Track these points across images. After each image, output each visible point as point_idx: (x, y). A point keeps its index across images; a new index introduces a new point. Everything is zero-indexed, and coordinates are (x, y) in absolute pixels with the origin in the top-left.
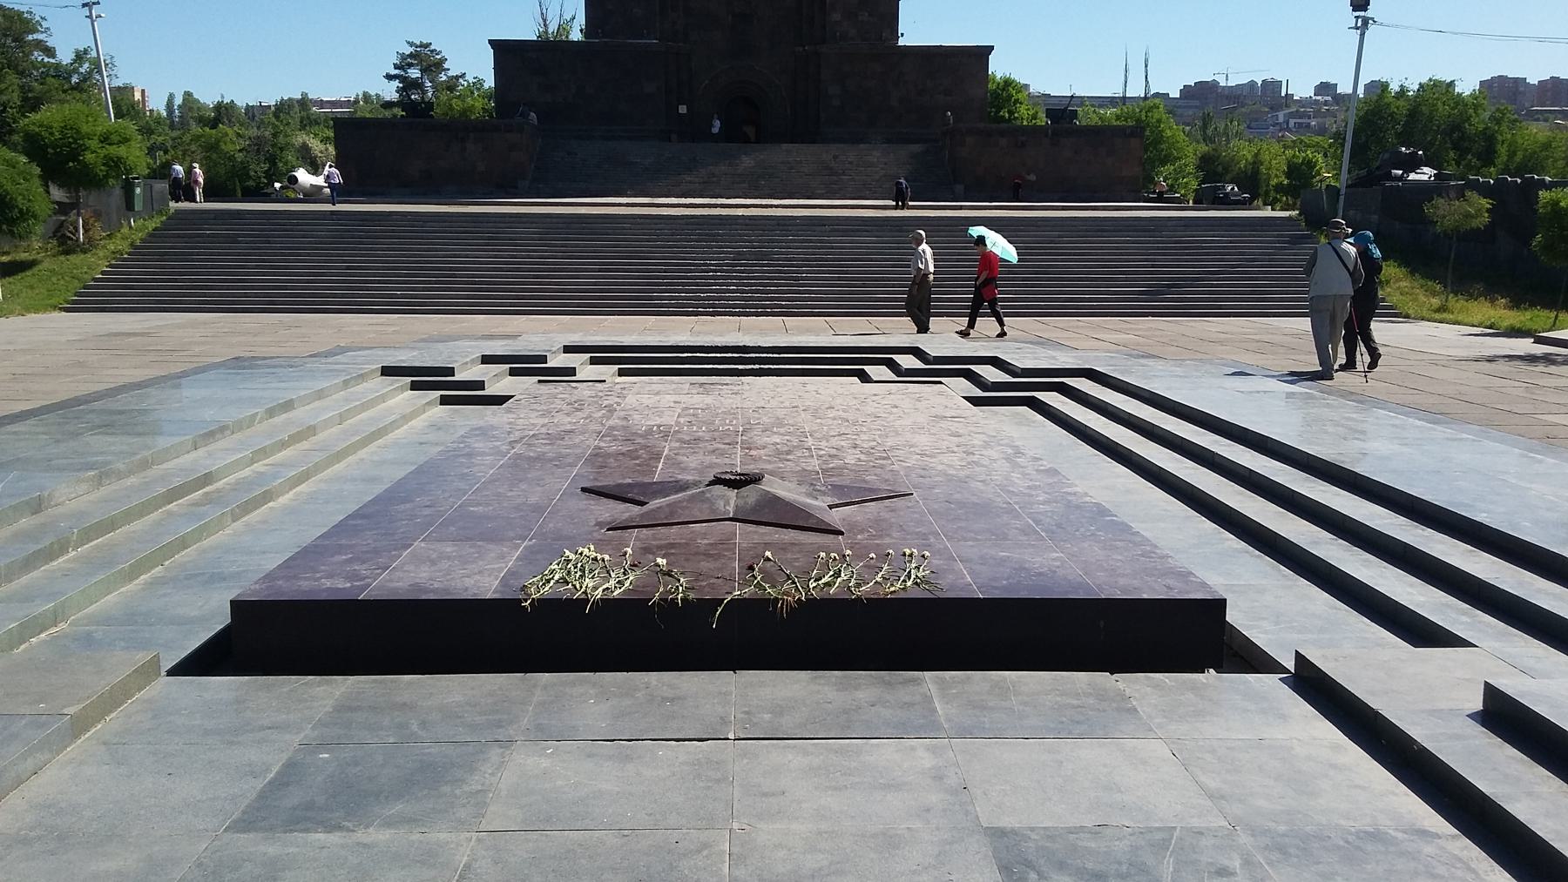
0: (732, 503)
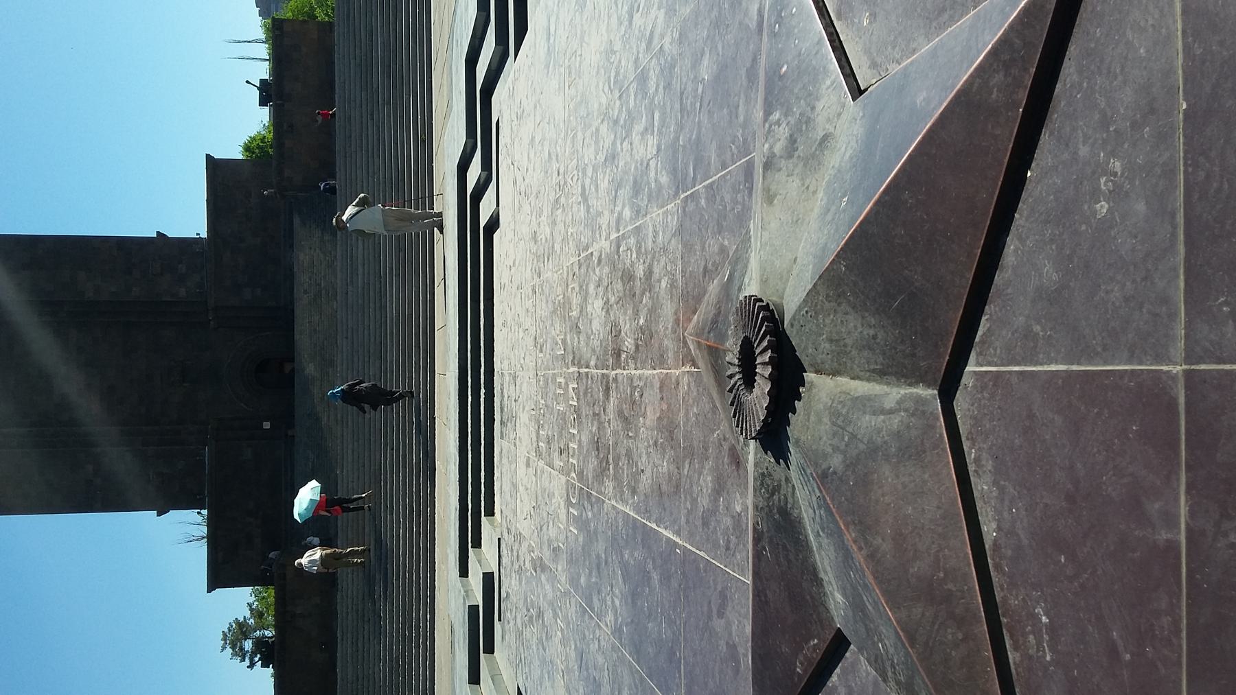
0: (861, 388)
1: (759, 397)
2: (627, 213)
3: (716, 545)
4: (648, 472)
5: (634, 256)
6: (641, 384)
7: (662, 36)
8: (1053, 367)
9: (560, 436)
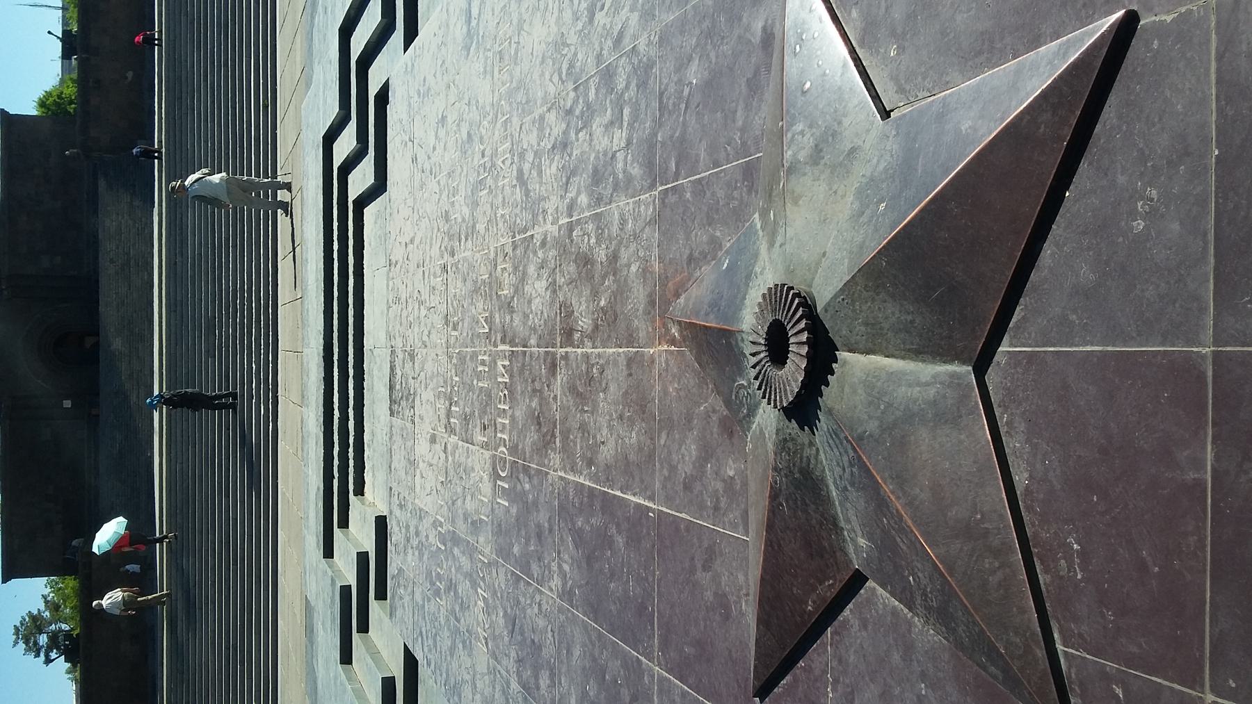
1: (793, 372)
2: (583, 199)
3: (702, 507)
4: (611, 444)
5: (593, 241)
6: (601, 362)
7: (635, 37)
8: (1089, 348)
9: (483, 412)
